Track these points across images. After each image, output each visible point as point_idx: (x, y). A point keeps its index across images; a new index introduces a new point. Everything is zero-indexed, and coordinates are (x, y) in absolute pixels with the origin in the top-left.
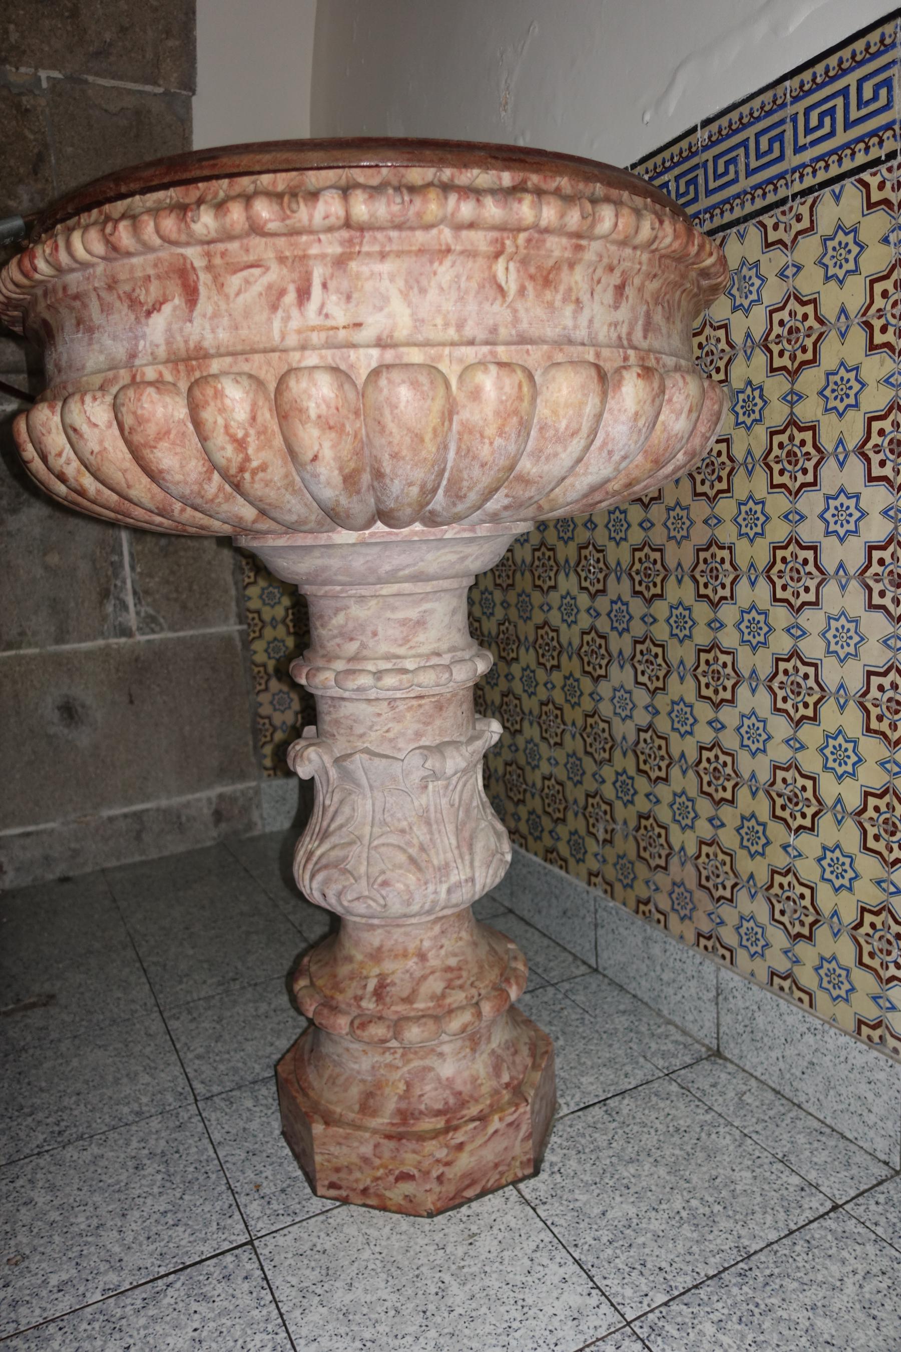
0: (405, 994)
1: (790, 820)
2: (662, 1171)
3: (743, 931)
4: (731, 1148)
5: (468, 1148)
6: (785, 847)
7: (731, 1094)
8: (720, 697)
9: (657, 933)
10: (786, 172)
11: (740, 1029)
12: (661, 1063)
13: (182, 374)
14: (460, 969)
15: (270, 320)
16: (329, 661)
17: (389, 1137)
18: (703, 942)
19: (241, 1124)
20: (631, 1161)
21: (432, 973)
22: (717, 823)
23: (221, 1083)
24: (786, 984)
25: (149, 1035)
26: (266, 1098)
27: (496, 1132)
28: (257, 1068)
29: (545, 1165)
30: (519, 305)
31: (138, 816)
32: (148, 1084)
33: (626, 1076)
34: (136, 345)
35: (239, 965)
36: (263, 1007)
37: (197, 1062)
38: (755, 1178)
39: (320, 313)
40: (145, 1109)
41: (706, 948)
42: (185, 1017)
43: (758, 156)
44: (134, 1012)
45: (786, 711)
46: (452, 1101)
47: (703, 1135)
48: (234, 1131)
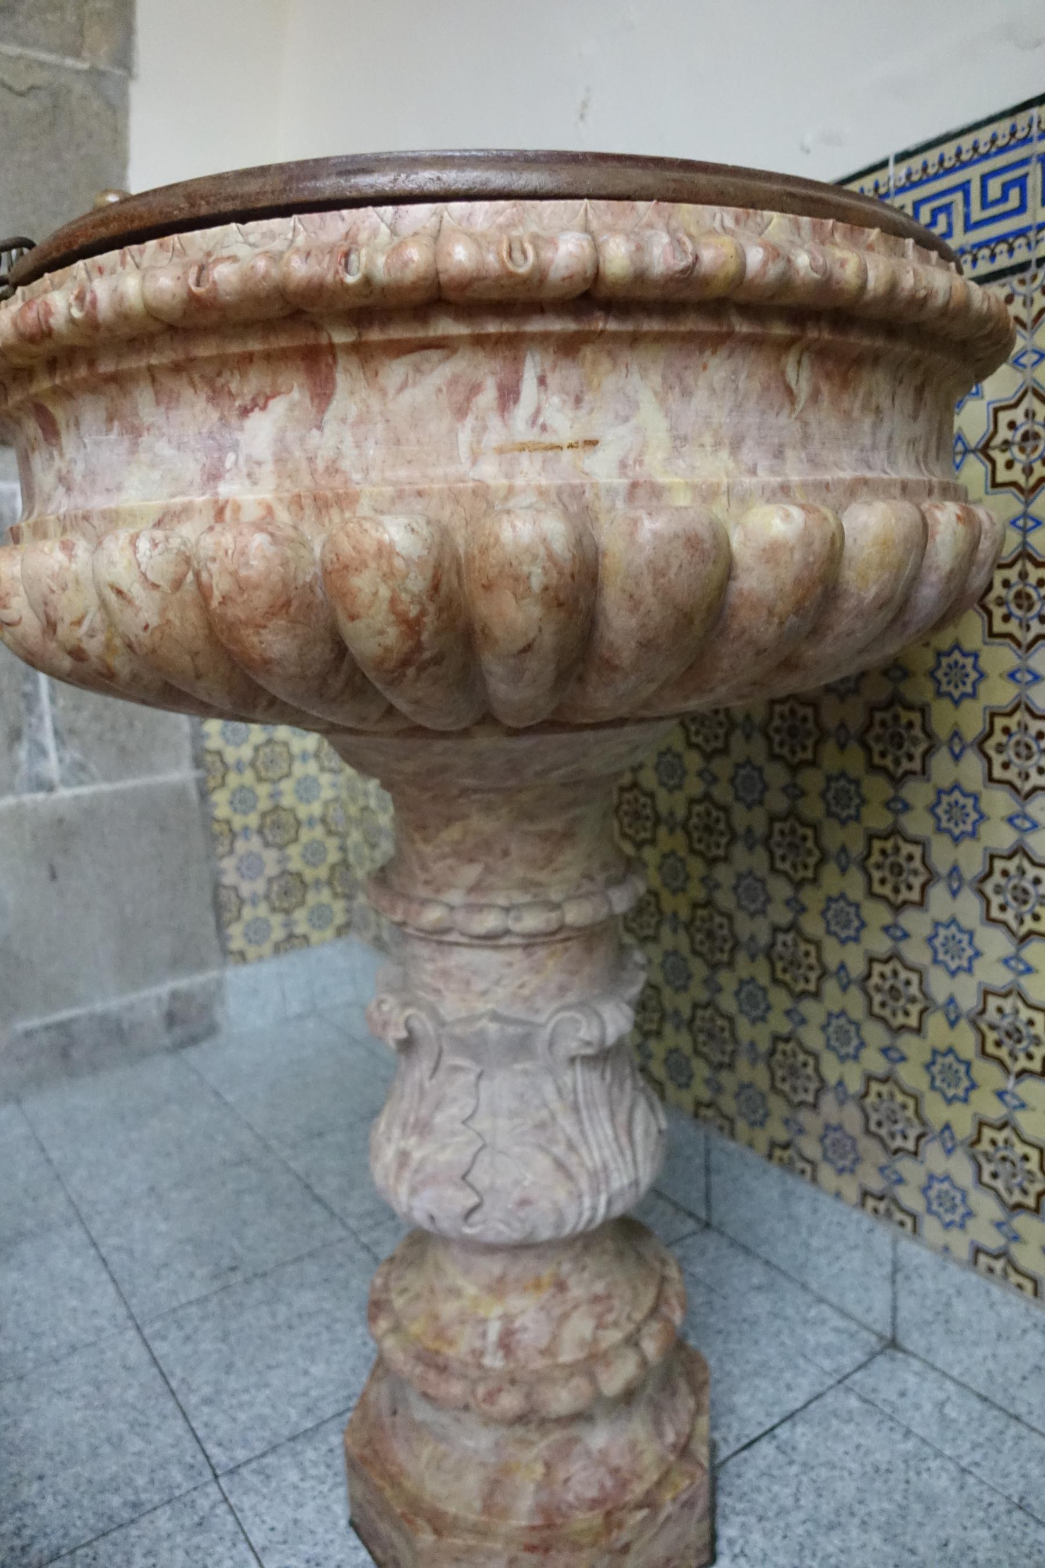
0: (544, 1343)
1: (1008, 1061)
2: (876, 1539)
3: (932, 1193)
4: (953, 1492)
5: (635, 1548)
6: (1000, 1095)
7: (928, 1407)
8: (901, 898)
9: (804, 1188)
10: (1029, 228)
11: (929, 1316)
12: (827, 1364)
13: (308, 511)
14: (609, 1296)
15: (452, 431)
16: (438, 891)
17: (531, 1548)
18: (871, 1203)
19: (290, 1514)
20: (831, 1527)
21: (576, 1307)
22: (894, 1055)
23: (246, 1444)
24: (999, 1265)
25: (127, 1368)
26: (315, 1464)
27: (668, 1518)
28: (293, 1414)
29: (722, 1545)
30: (811, 418)
31: (63, 1027)
32: (140, 1454)
33: (789, 1387)
34: (221, 460)
35: (235, 1244)
36: (282, 1311)
37: (206, 1410)
38: (995, 1537)
39: (534, 423)
40: (144, 1496)
41: (876, 1211)
42: (175, 1334)
43: (985, 205)
44: (99, 1330)
45: (1005, 924)
46: (609, 1483)
47: (912, 1474)
48: (280, 1527)
